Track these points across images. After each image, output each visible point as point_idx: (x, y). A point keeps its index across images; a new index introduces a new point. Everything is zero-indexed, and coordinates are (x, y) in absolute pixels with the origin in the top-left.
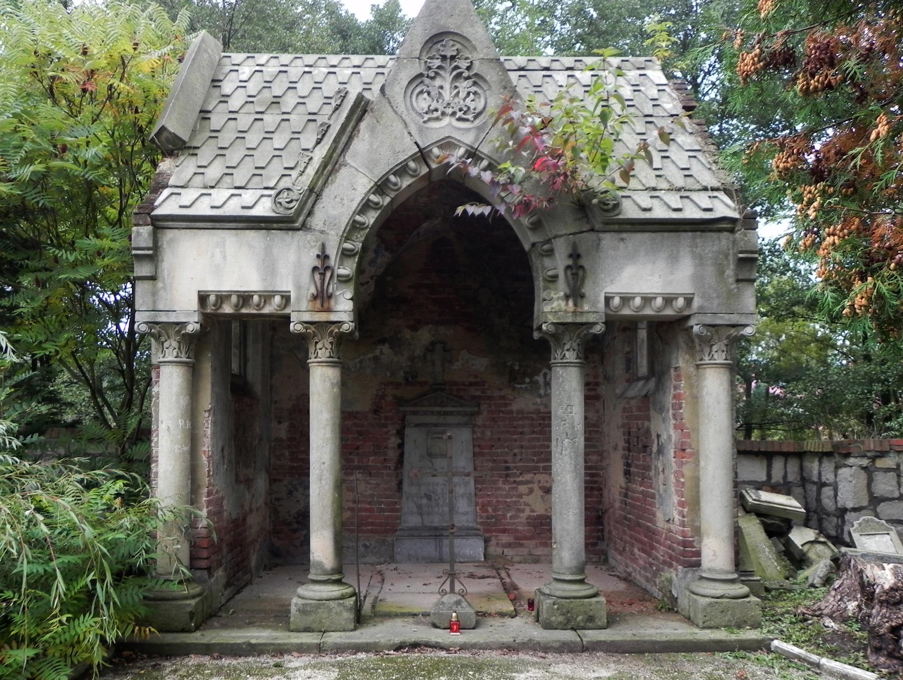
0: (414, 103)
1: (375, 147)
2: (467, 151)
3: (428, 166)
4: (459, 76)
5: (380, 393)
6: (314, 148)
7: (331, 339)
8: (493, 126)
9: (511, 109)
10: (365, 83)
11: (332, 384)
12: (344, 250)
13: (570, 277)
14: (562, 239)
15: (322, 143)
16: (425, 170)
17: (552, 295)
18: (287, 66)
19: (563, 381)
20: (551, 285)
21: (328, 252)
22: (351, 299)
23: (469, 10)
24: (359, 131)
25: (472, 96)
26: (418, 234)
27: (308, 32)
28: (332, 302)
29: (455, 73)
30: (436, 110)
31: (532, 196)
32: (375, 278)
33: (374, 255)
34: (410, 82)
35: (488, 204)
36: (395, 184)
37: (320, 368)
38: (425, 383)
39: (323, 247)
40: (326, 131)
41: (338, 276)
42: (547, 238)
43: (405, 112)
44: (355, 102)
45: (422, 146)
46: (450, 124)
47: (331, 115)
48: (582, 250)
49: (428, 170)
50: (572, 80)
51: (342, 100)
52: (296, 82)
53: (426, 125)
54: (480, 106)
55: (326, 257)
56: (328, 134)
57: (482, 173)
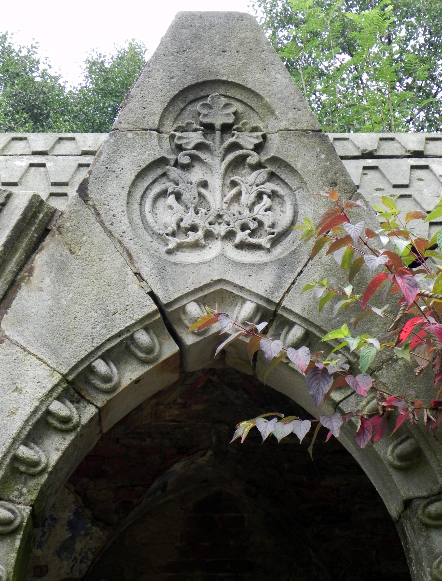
0: (149, 216)
1: (64, 302)
2: (258, 308)
3: (178, 340)
10: (54, 184)
24: (31, 271)
25: (266, 201)
26: (164, 488)
29: (231, 157)
30: (194, 228)
31: (397, 399)
33: (69, 535)
34: (140, 176)
35: (309, 416)
36: (107, 379)
43: (129, 233)
44: (25, 215)
45: (164, 299)
46: (222, 256)
53: (172, 258)
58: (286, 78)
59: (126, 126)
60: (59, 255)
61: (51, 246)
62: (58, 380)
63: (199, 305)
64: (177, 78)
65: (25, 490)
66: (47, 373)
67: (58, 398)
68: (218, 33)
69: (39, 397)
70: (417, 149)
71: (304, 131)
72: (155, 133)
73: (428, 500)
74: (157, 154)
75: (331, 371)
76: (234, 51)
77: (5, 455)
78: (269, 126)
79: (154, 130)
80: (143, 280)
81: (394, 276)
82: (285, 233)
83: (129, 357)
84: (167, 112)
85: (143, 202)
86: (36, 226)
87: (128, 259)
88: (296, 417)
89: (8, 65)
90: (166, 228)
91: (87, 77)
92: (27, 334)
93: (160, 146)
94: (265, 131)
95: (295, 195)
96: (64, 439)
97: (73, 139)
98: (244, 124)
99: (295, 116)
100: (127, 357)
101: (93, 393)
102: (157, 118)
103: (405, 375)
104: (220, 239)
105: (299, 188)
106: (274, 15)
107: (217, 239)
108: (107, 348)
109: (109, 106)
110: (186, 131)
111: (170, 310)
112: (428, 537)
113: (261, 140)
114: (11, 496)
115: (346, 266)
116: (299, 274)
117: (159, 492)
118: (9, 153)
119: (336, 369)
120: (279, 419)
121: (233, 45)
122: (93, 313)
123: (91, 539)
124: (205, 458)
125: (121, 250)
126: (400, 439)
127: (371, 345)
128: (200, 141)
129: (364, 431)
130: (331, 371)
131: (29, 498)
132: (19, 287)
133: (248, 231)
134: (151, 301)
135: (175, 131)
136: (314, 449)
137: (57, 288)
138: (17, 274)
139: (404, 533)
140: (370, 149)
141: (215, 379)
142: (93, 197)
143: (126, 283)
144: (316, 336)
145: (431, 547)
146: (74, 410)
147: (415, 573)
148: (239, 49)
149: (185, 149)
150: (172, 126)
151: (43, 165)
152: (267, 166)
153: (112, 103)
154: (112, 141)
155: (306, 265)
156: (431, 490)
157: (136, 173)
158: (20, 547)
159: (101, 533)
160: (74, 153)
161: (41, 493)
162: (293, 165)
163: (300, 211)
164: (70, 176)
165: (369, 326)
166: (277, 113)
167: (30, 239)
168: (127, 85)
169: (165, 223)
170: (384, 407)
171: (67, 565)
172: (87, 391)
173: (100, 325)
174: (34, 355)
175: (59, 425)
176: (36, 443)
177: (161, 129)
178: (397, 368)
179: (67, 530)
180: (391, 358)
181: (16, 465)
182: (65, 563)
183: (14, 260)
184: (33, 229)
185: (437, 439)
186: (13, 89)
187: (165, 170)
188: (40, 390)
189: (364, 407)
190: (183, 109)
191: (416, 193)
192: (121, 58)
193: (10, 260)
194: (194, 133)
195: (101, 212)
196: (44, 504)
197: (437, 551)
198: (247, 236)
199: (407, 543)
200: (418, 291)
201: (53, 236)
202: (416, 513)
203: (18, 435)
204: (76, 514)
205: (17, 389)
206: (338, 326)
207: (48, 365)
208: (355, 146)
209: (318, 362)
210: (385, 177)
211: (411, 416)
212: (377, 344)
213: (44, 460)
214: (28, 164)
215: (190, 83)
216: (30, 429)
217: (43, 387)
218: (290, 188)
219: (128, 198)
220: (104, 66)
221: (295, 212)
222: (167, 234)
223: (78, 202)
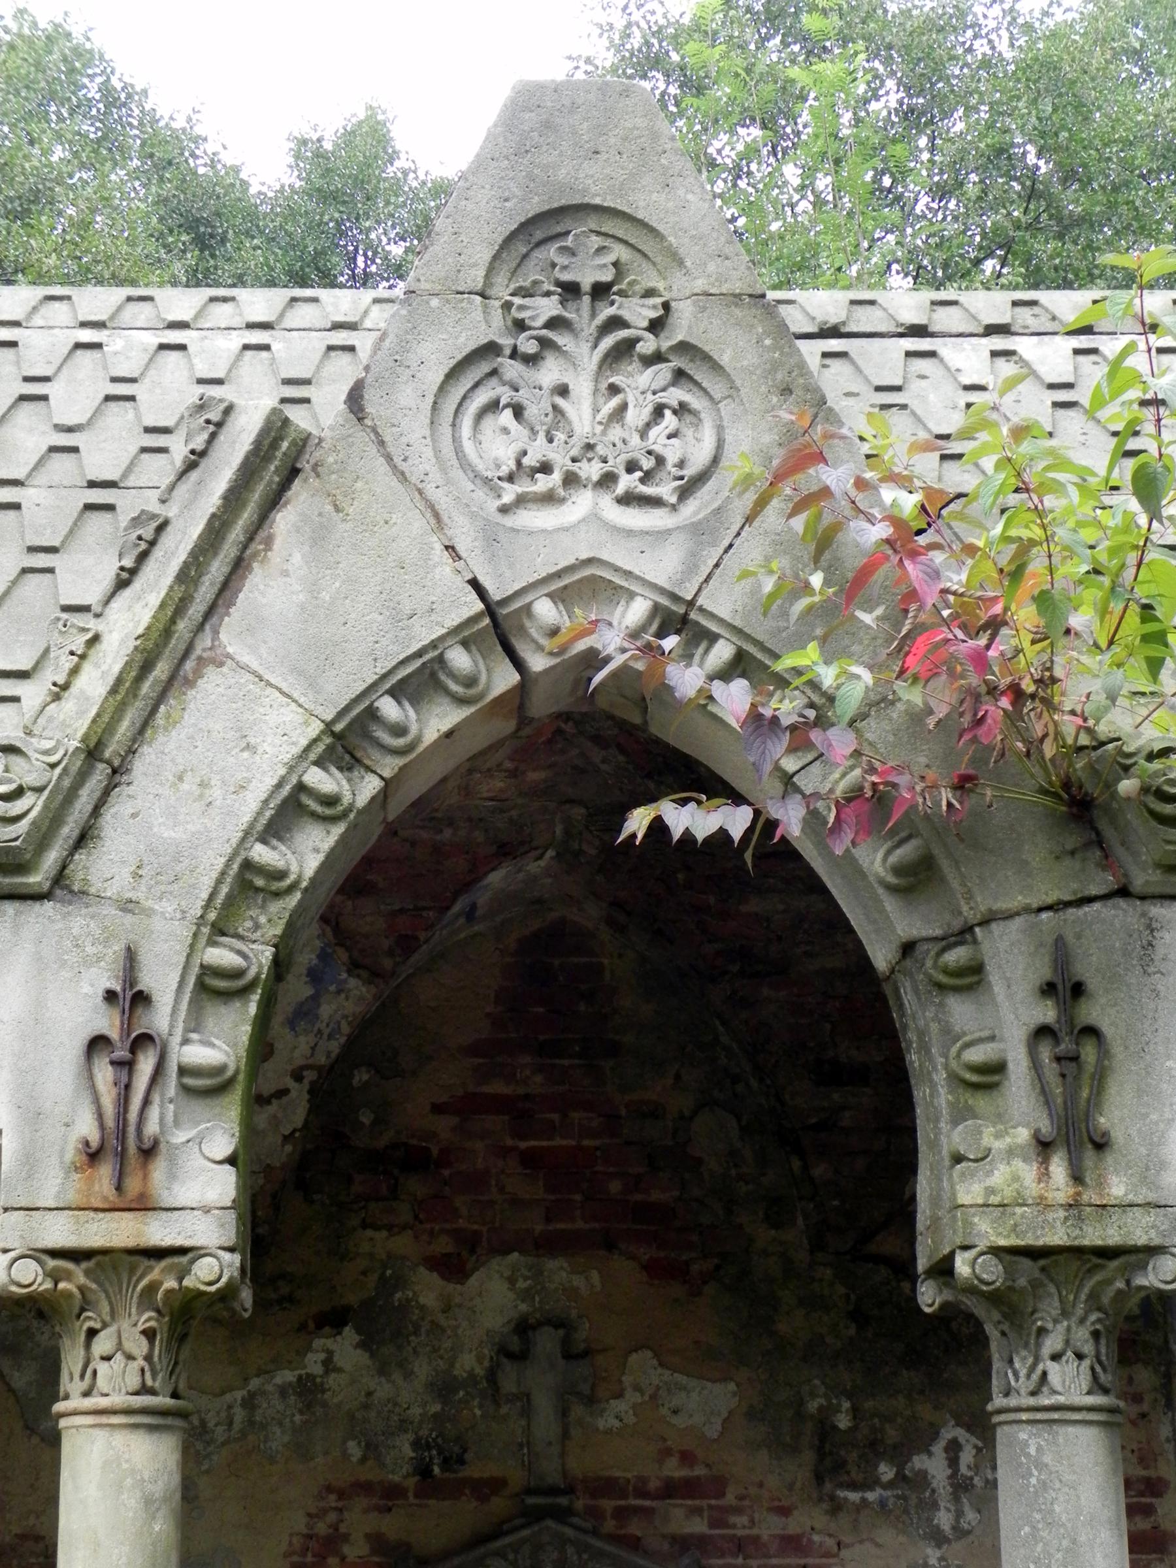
0: (468, 446)
1: (326, 596)
2: (656, 608)
3: (518, 664)
4: (624, 350)
5: (322, 1528)
6: (108, 601)
7: (147, 1319)
8: (749, 520)
9: (820, 458)
10: (288, 382)
11: (148, 1501)
12: (208, 970)
13: (1051, 1070)
14: (1018, 922)
15: (137, 584)
16: (505, 679)
17: (987, 1139)
18: (16, 324)
19: (1044, 1486)
20: (980, 1102)
21: (147, 981)
22: (231, 1160)
23: (655, 136)
24: (269, 542)
25: (669, 419)
26: (470, 914)
27: (84, 225)
28: (158, 1170)
29: (608, 342)
30: (545, 468)
31: (899, 769)
32: (310, 1076)
33: (308, 991)
34: (453, 374)
35: (738, 799)
36: (399, 730)
37: (100, 1434)
38: (496, 1485)
39: (131, 957)
40: (152, 543)
41: (183, 1071)
42: (957, 925)
43: (436, 476)
44: (258, 443)
45: (496, 593)
46: (595, 517)
47: (172, 487)
48: (1086, 969)
49: (515, 678)
50: (1007, 368)
51: (213, 436)
52: (46, 379)
53: (509, 521)
54: (700, 457)
55: (141, 999)
56: (158, 553)
57: (717, 688)
58: (705, 201)
59: (428, 286)
60: (316, 513)
61: (302, 498)
62: (317, 732)
63: (555, 603)
64: (515, 200)
65: (263, 920)
66: (300, 719)
67: (317, 763)
68: (586, 119)
69: (286, 760)
70: (916, 321)
71: (735, 296)
72: (478, 298)
73: (944, 943)
74: (482, 337)
75: (786, 721)
76: (613, 152)
77: (230, 860)
78: (675, 288)
79: (476, 294)
80: (460, 558)
81: (901, 560)
82: (701, 478)
83: (436, 691)
84: (498, 262)
85: (458, 421)
86: (277, 463)
87: (433, 521)
88: (726, 801)
89: (152, 146)
90: (498, 467)
91: (291, 167)
92: (263, 651)
93: (487, 322)
94: (667, 296)
95: (719, 410)
96: (328, 832)
97: (315, 300)
98: (631, 284)
99: (720, 270)
100: (432, 692)
101: (375, 754)
102: (481, 273)
103: (908, 728)
104: (590, 486)
105: (726, 398)
106: (627, 55)
107: (585, 486)
108: (399, 677)
109: (331, 220)
110: (531, 296)
111: (505, 611)
112: (941, 1005)
113: (661, 312)
114: (240, 930)
115: (809, 537)
116: (726, 551)
117: (462, 920)
118: (207, 326)
119: (795, 719)
120: (699, 803)
121: (612, 141)
122: (376, 616)
123: (347, 998)
124: (542, 863)
125: (421, 505)
126: (897, 838)
127: (858, 677)
128: (555, 313)
129: (840, 824)
130: (786, 721)
131: (271, 933)
132: (249, 568)
133: (639, 474)
134: (474, 596)
135: (512, 295)
136: (753, 855)
137: (314, 570)
138: (245, 547)
139: (898, 997)
140: (833, 320)
141: (569, 728)
142: (373, 411)
143: (430, 563)
144: (755, 658)
145: (947, 1022)
146: (344, 782)
147: (916, 1065)
148: (622, 149)
149: (530, 328)
150: (507, 286)
151: (266, 348)
152: (671, 358)
153: (337, 215)
154: (404, 312)
155: (738, 534)
156: (949, 925)
157: (446, 370)
158: (256, 1015)
159: (364, 989)
160: (318, 326)
161: (290, 925)
162: (715, 357)
163: (729, 438)
164: (313, 368)
165: (847, 642)
166: (688, 264)
167: (267, 486)
168: (362, 182)
169: (496, 459)
170: (874, 784)
171: (304, 1044)
172: (365, 750)
173: (388, 636)
174: (277, 688)
175: (319, 809)
176: (280, 839)
177: (489, 292)
178: (895, 715)
179: (306, 983)
180: (884, 699)
181: (248, 876)
182: (302, 1039)
183: (241, 522)
184: (272, 468)
185: (962, 840)
186: (162, 189)
187: (495, 365)
188: (288, 749)
189: (837, 782)
190: (525, 256)
191: (916, 402)
192: (352, 133)
193: (234, 522)
194: (545, 299)
195: (387, 439)
196: (291, 943)
197: (957, 1029)
198: (637, 483)
199: (903, 1015)
200: (942, 586)
201: (305, 480)
202: (923, 965)
203: (252, 825)
204: (323, 956)
205: (248, 746)
206: (799, 643)
207: (300, 706)
208: (808, 314)
209: (763, 705)
210: (861, 372)
211: (921, 800)
212: (867, 677)
213: (294, 868)
214: (240, 346)
215: (538, 210)
216: (272, 816)
217: (293, 744)
218: (711, 398)
219: (432, 414)
220: (321, 147)
221: (719, 440)
222: (500, 478)
223: (346, 420)
